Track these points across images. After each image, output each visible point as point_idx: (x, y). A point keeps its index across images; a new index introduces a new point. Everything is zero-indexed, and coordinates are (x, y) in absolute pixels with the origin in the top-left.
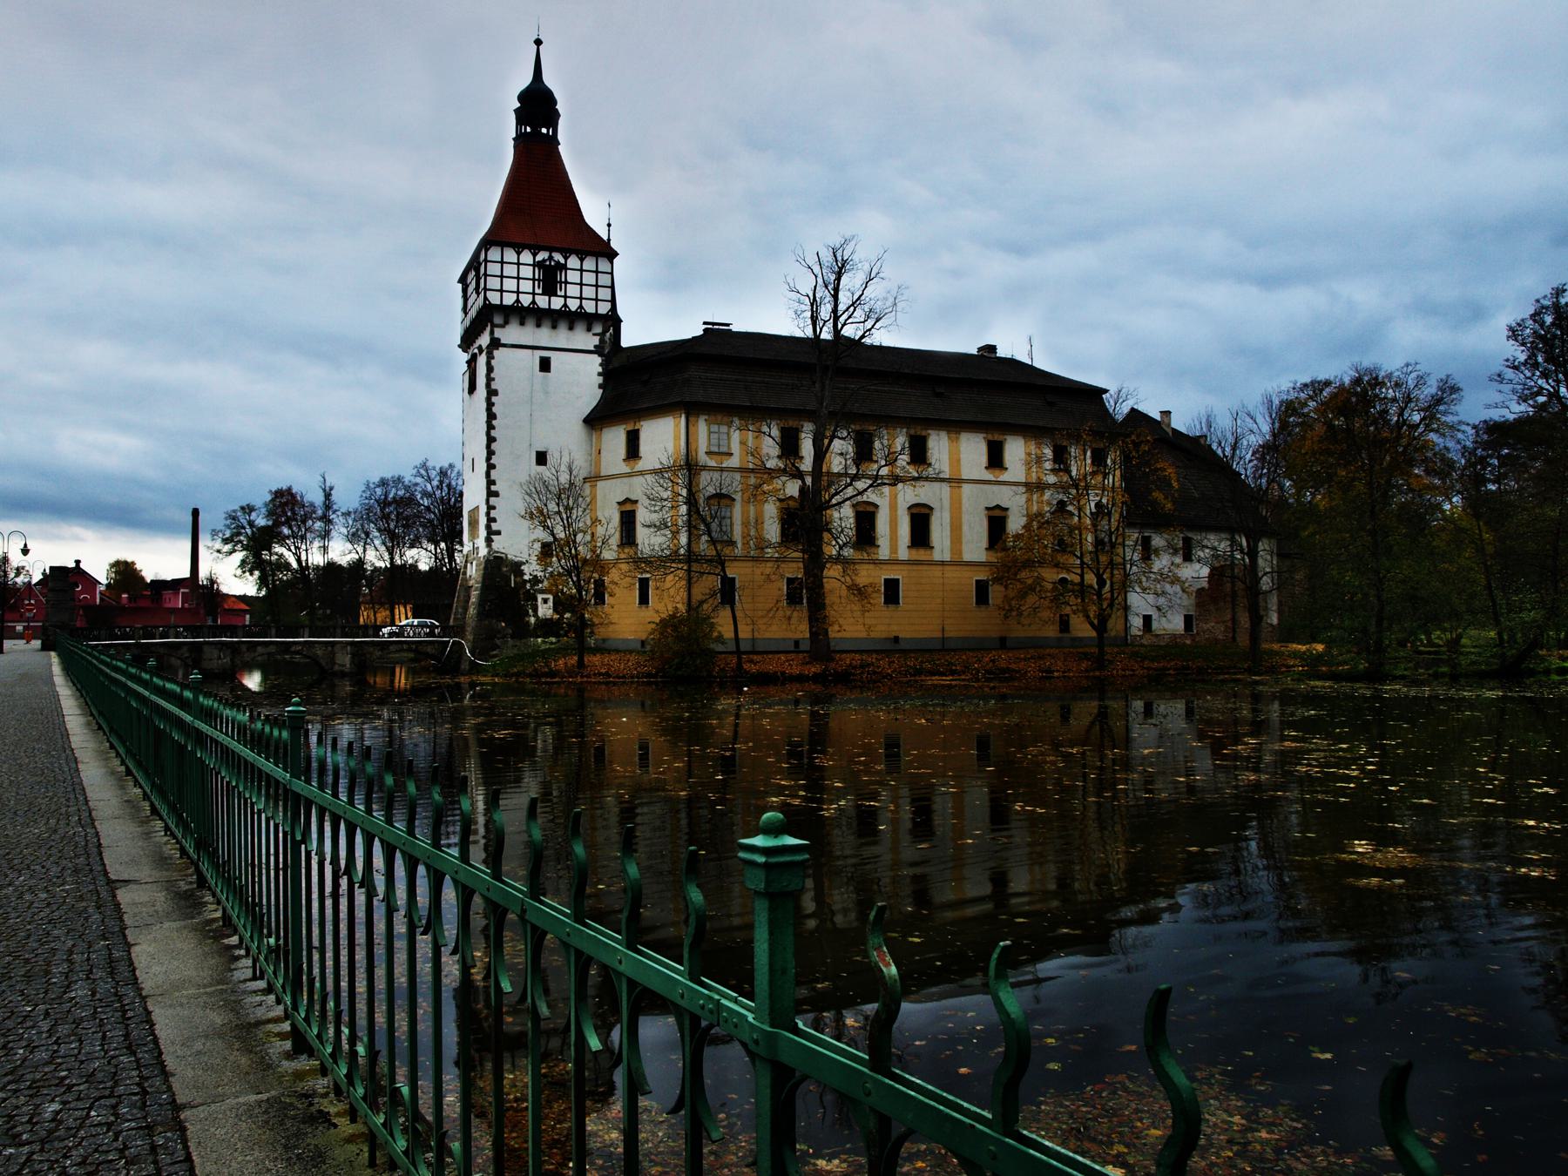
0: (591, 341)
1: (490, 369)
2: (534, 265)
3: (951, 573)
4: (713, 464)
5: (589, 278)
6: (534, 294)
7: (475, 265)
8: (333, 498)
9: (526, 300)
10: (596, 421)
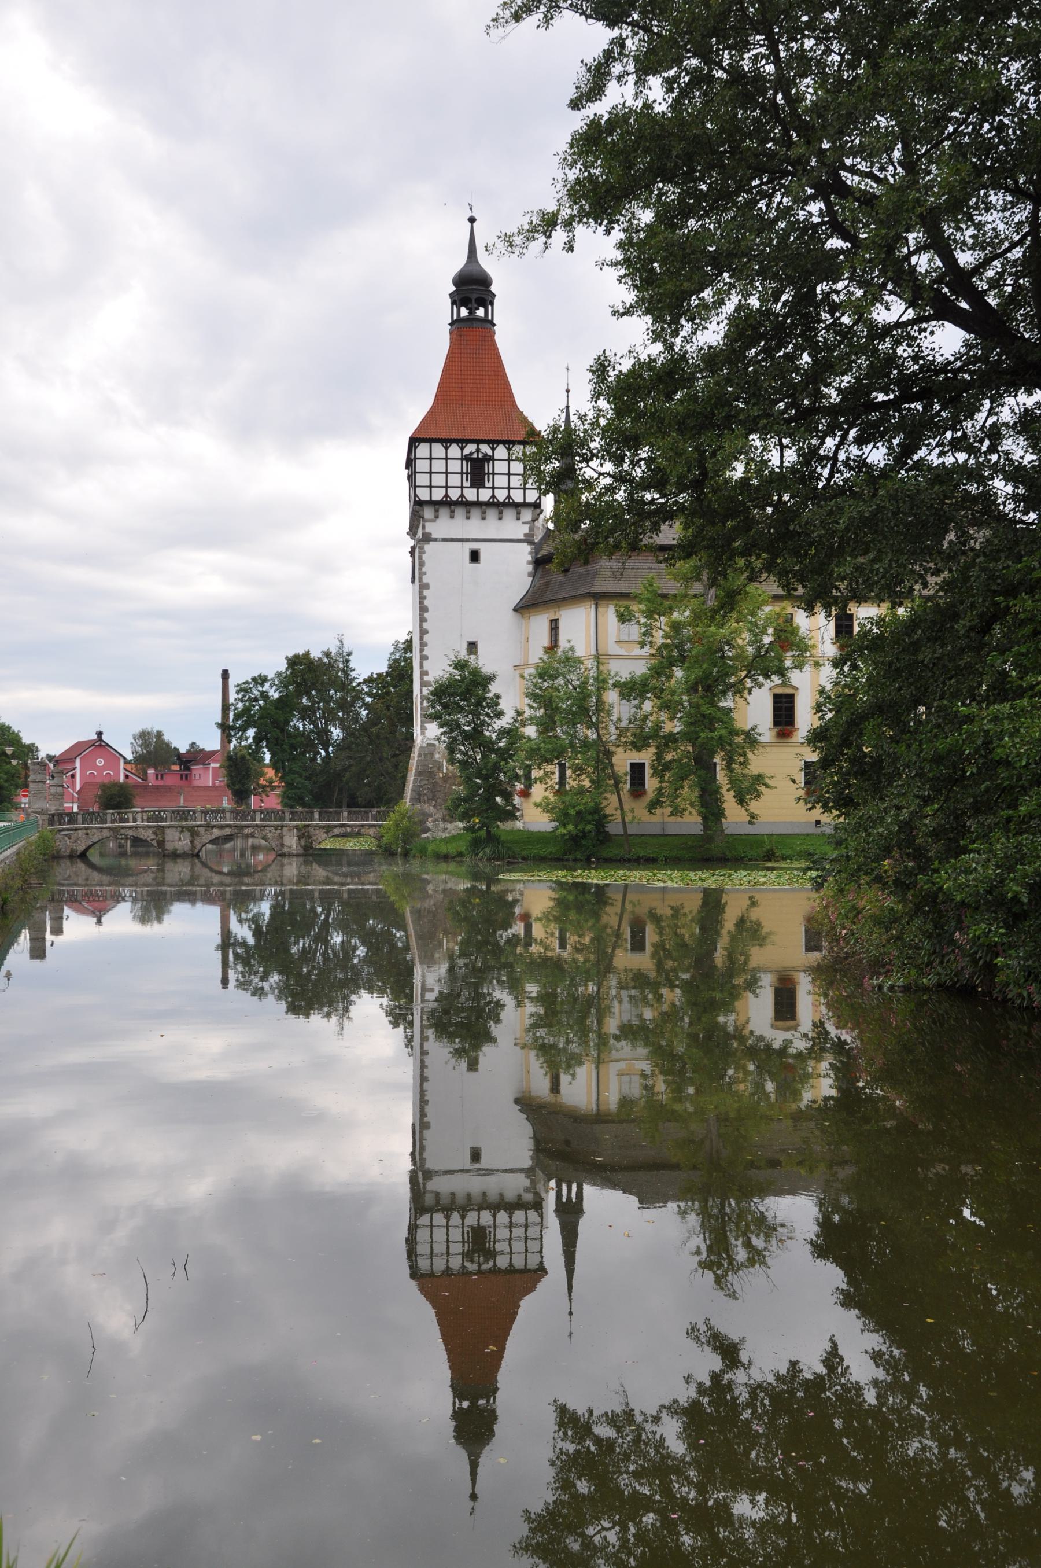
0: (520, 530)
2: (462, 459)
4: (622, 652)
6: (462, 487)
8: (352, 665)
9: (454, 495)
10: (526, 607)
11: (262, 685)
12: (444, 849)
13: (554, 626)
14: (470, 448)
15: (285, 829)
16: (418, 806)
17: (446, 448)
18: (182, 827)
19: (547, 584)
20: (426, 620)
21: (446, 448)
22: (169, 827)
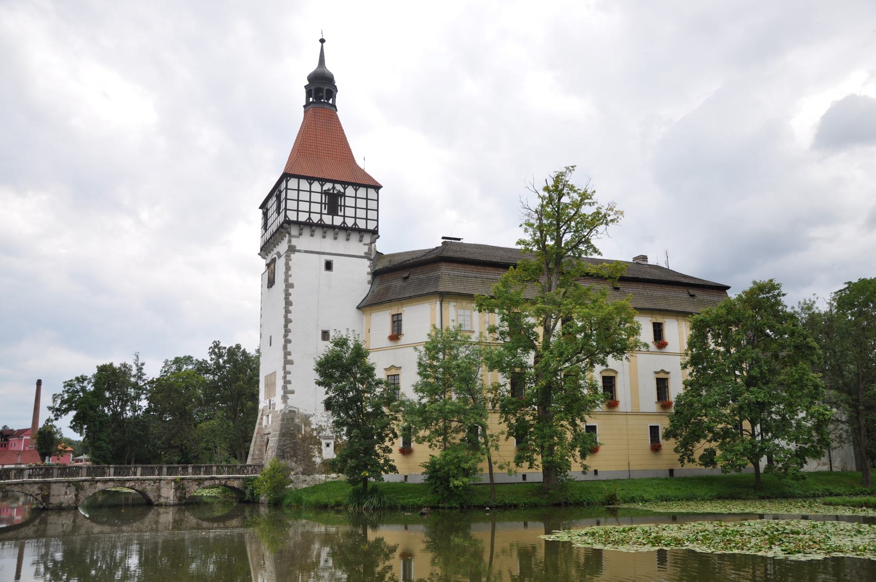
0: (362, 249)
1: (288, 268)
3: (632, 420)
5: (361, 203)
6: (321, 213)
7: (276, 192)
8: (144, 371)
9: (315, 218)
10: (367, 306)
11: (83, 382)
12: (323, 497)
13: (397, 322)
14: (328, 186)
15: (162, 482)
16: (283, 462)
17: (310, 184)
18: (69, 482)
19: (388, 289)
20: (290, 312)
21: (310, 184)
22: (55, 482)
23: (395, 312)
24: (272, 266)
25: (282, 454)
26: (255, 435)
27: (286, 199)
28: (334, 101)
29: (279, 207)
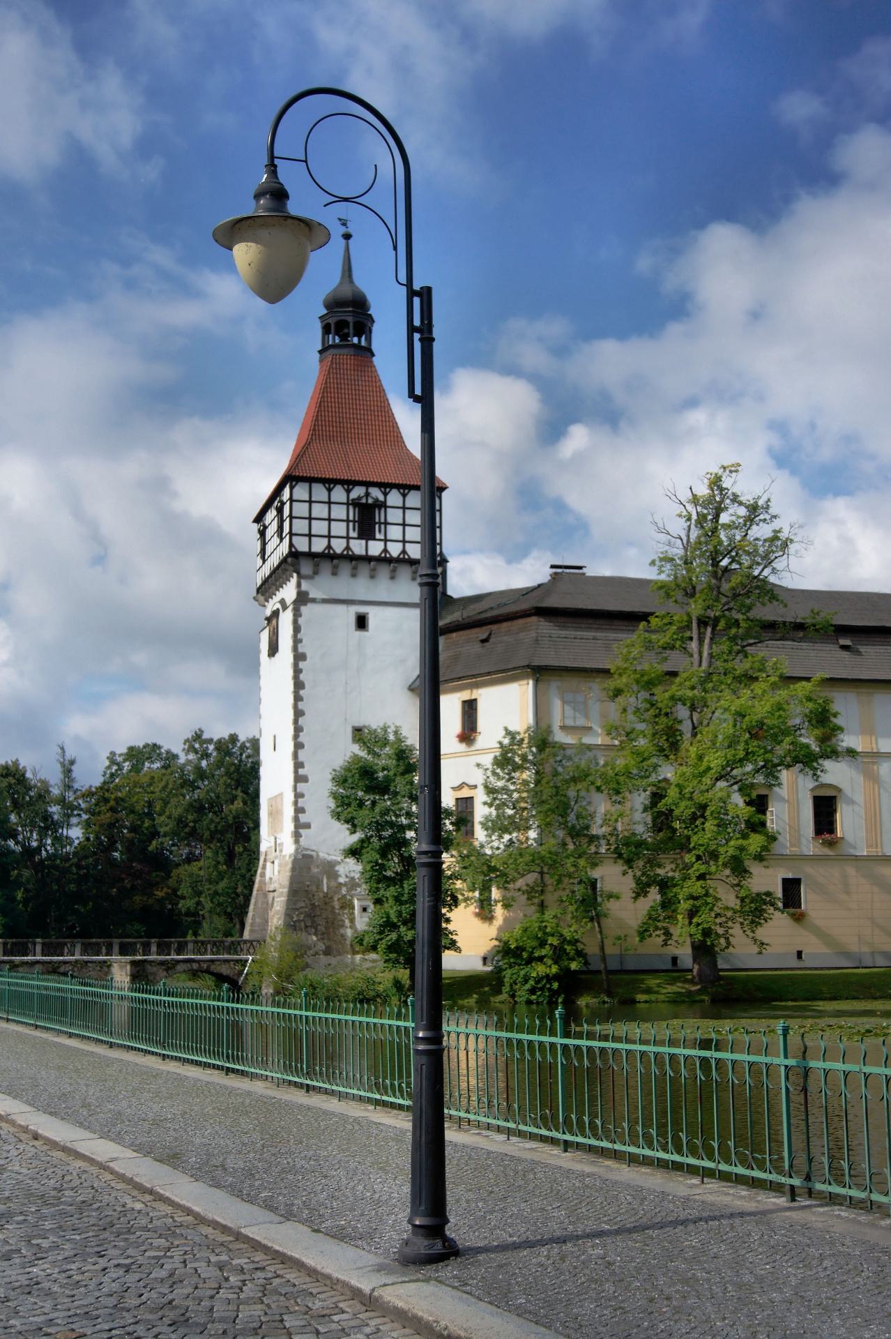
1: (297, 629)
6: (348, 538)
8: (74, 775)
9: (338, 546)
14: (358, 492)
17: (330, 490)
21: (330, 490)
23: (466, 695)
24: (274, 622)
25: (291, 925)
26: (255, 892)
27: (291, 517)
28: (369, 340)
29: (281, 528)
